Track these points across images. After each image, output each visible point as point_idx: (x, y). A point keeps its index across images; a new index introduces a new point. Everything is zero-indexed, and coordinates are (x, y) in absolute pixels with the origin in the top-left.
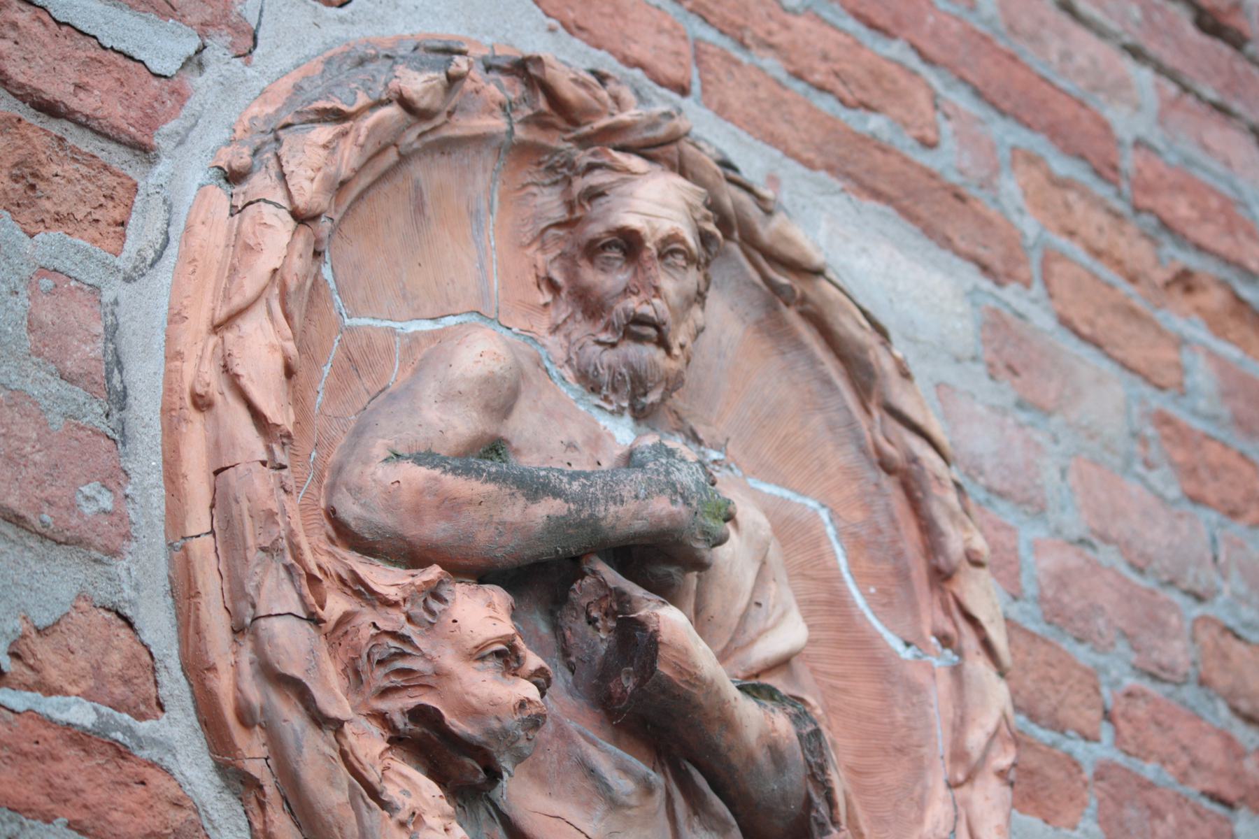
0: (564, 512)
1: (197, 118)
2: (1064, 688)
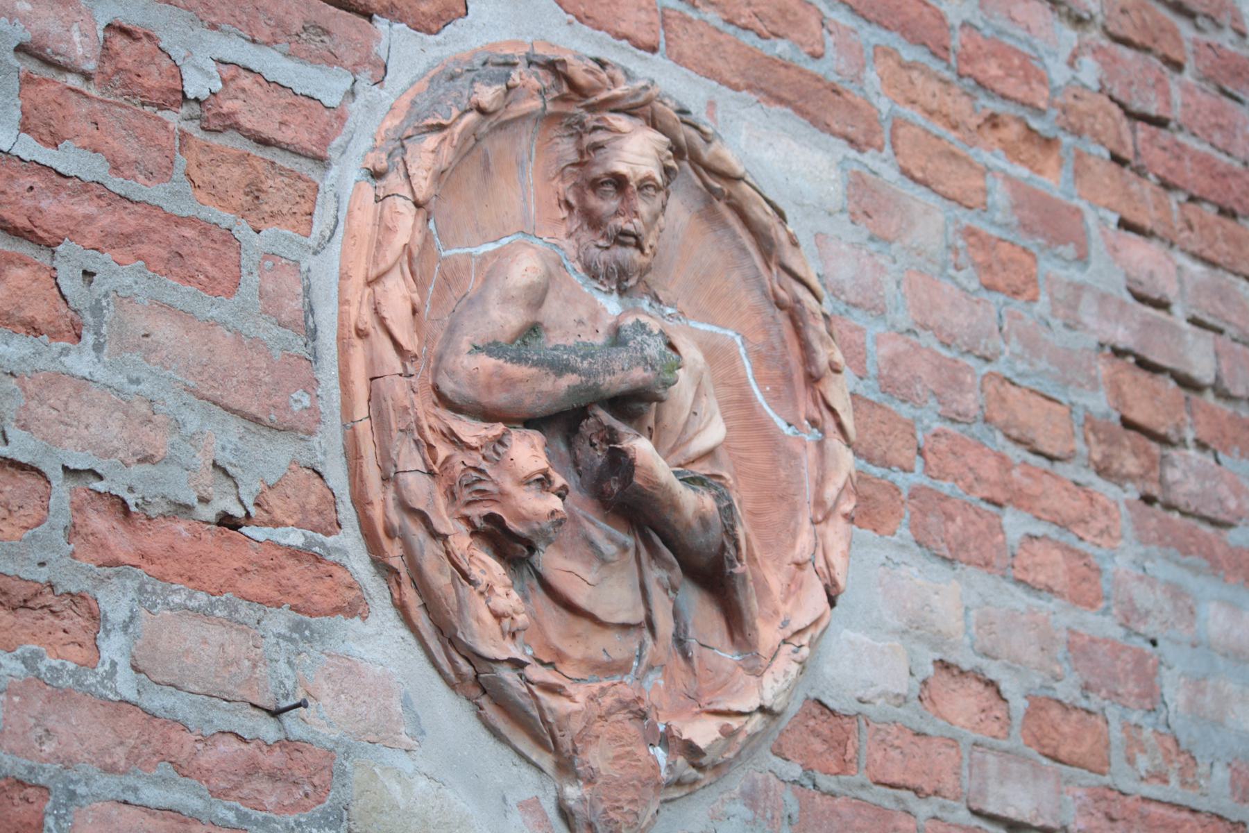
0: (578, 382)
1: (352, 133)
2: (891, 438)
